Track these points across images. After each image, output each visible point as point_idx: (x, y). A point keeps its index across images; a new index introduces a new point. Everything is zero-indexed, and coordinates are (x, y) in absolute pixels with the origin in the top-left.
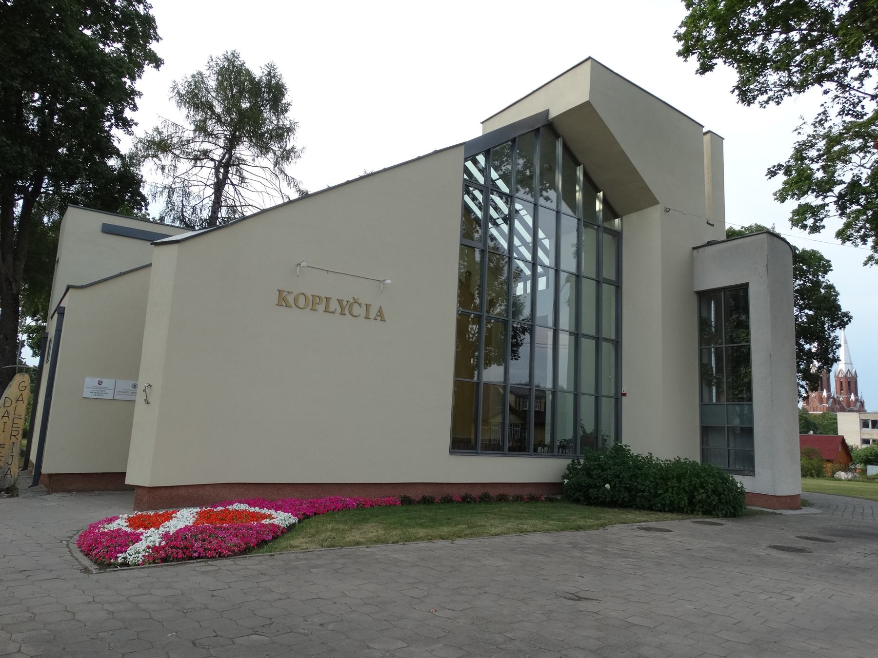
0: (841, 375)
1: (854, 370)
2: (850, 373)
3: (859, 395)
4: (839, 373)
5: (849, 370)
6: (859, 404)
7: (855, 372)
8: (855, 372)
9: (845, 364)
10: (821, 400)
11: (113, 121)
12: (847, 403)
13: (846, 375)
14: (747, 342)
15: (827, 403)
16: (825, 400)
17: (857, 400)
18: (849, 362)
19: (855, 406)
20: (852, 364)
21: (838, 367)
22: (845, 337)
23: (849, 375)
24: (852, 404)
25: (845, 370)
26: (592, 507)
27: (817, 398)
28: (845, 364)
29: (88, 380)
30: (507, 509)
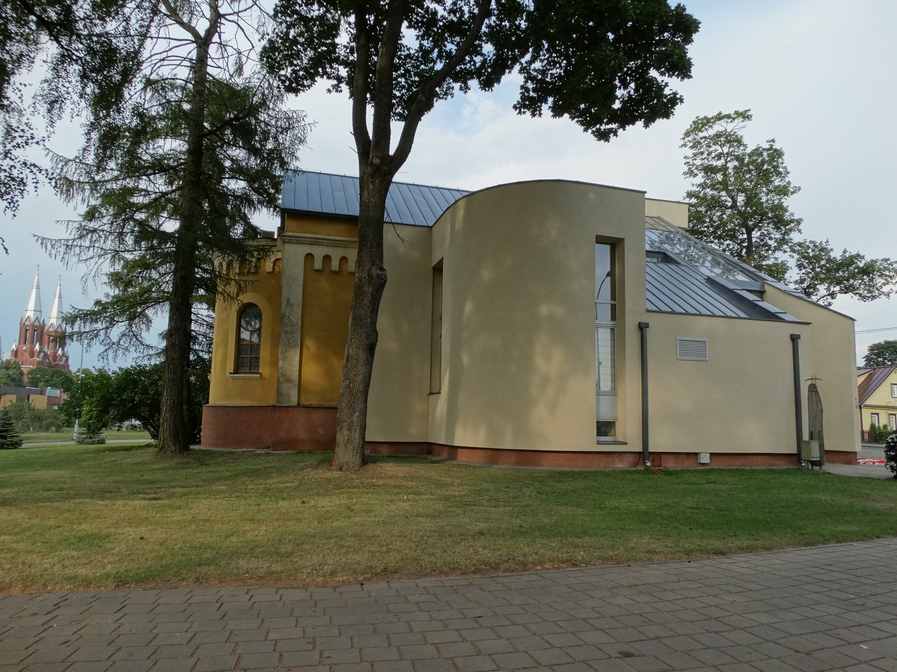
0: (28, 323)
1: (43, 318)
2: (38, 321)
3: (66, 350)
4: (26, 320)
5: (37, 318)
6: (42, 354)
7: (44, 320)
8: (44, 320)
9: (34, 311)
10: (32, 354)
11: (532, 94)
12: (53, 356)
13: (34, 323)
14: (258, 354)
15: (38, 357)
16: (36, 354)
17: (63, 354)
18: (39, 310)
19: (61, 361)
20: (41, 312)
21: (26, 313)
22: (38, 282)
23: (37, 324)
24: (58, 359)
25: (33, 318)
26: (390, 464)
27: (28, 351)
28: (34, 311)
29: (613, 36)
30: (419, 467)
